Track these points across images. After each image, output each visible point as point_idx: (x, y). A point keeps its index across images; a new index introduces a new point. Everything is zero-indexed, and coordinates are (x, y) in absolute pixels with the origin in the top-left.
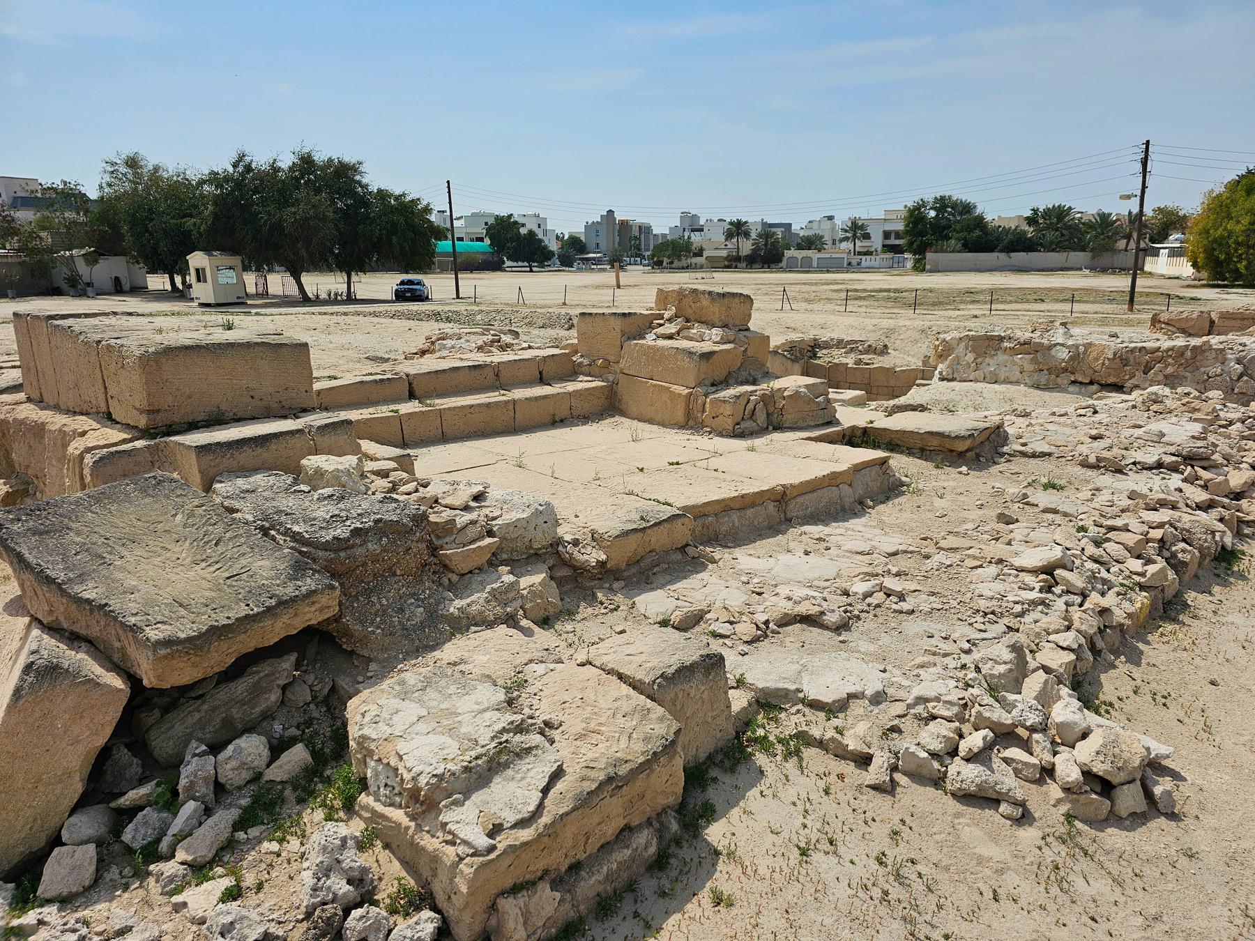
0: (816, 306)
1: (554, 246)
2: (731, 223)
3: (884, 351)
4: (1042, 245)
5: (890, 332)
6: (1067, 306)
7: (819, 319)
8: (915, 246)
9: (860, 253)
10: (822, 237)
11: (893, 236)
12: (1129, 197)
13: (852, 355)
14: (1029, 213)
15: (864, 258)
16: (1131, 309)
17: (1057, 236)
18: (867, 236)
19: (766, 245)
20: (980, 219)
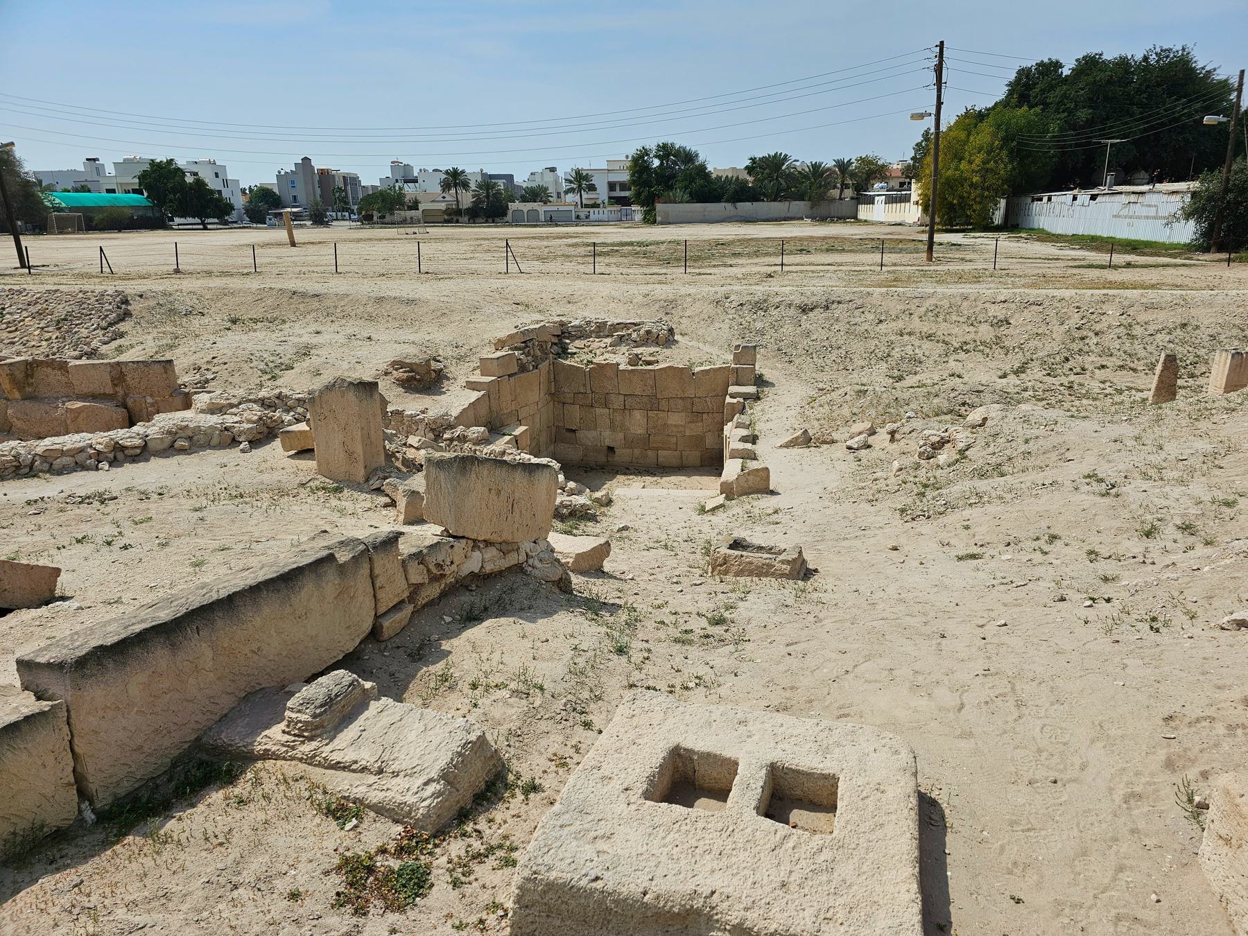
0: (553, 266)
1: (239, 202)
2: (447, 172)
3: (668, 340)
4: (764, 195)
5: (669, 305)
6: (877, 257)
7: (562, 287)
8: (643, 197)
9: (587, 206)
10: (546, 189)
11: (618, 188)
12: (921, 116)
13: (624, 349)
14: (748, 163)
15: (592, 210)
16: (930, 259)
17: (773, 186)
18: (592, 188)
19: (488, 196)
20: (702, 168)
